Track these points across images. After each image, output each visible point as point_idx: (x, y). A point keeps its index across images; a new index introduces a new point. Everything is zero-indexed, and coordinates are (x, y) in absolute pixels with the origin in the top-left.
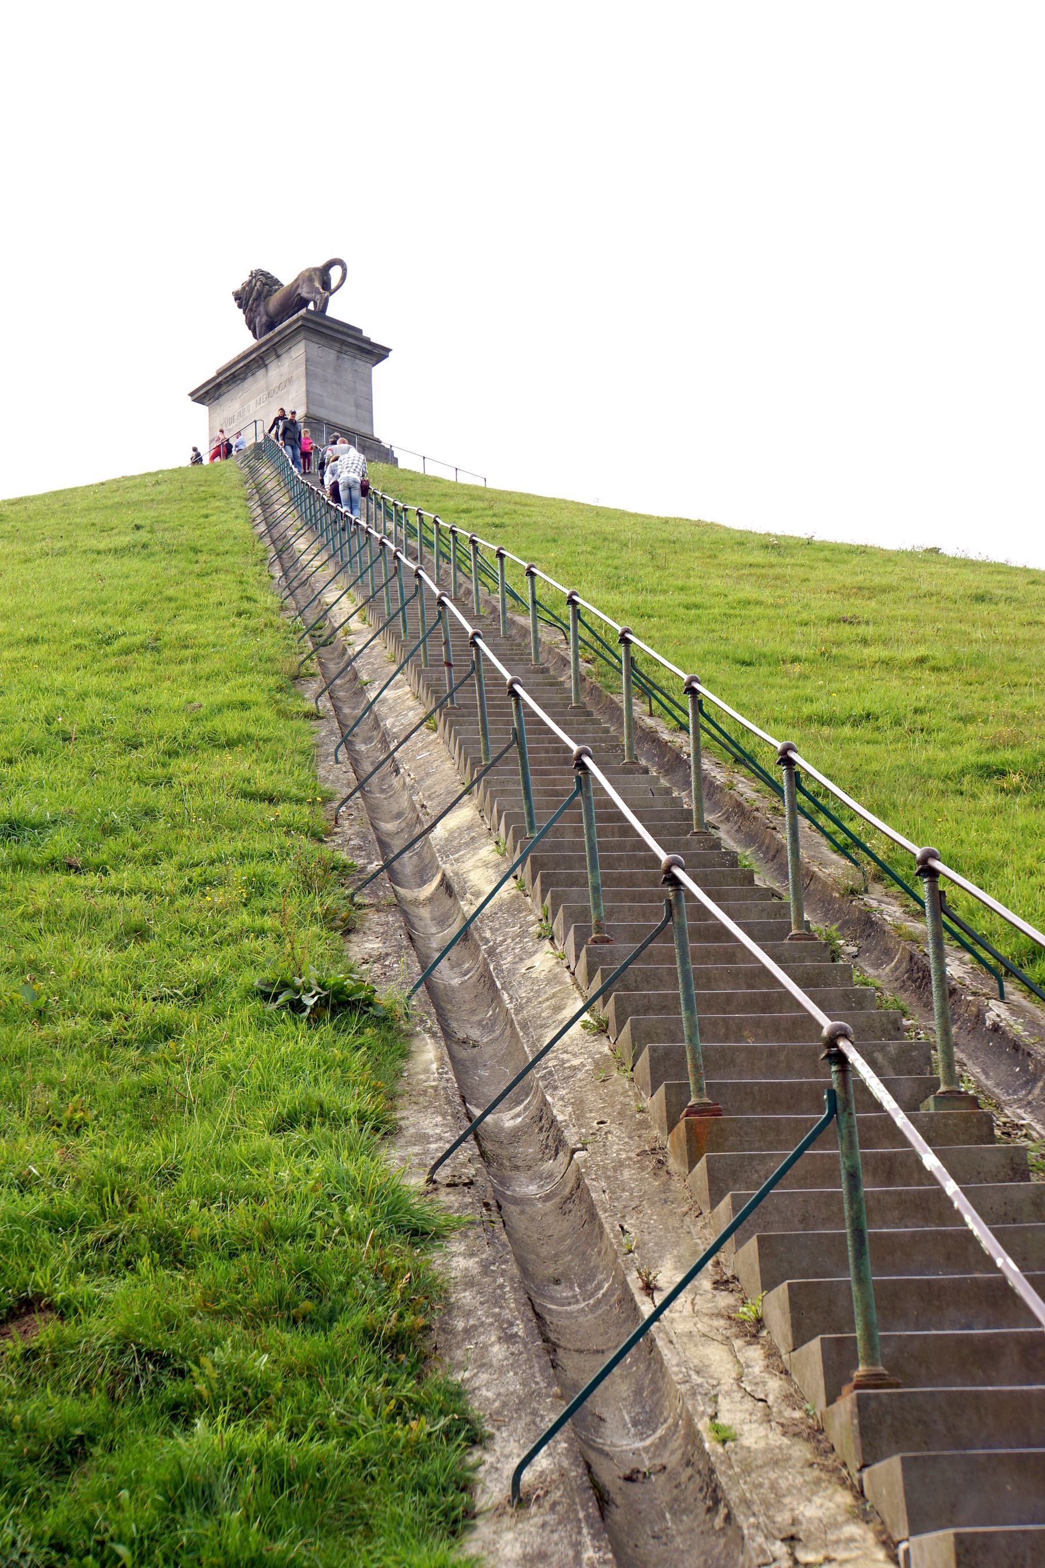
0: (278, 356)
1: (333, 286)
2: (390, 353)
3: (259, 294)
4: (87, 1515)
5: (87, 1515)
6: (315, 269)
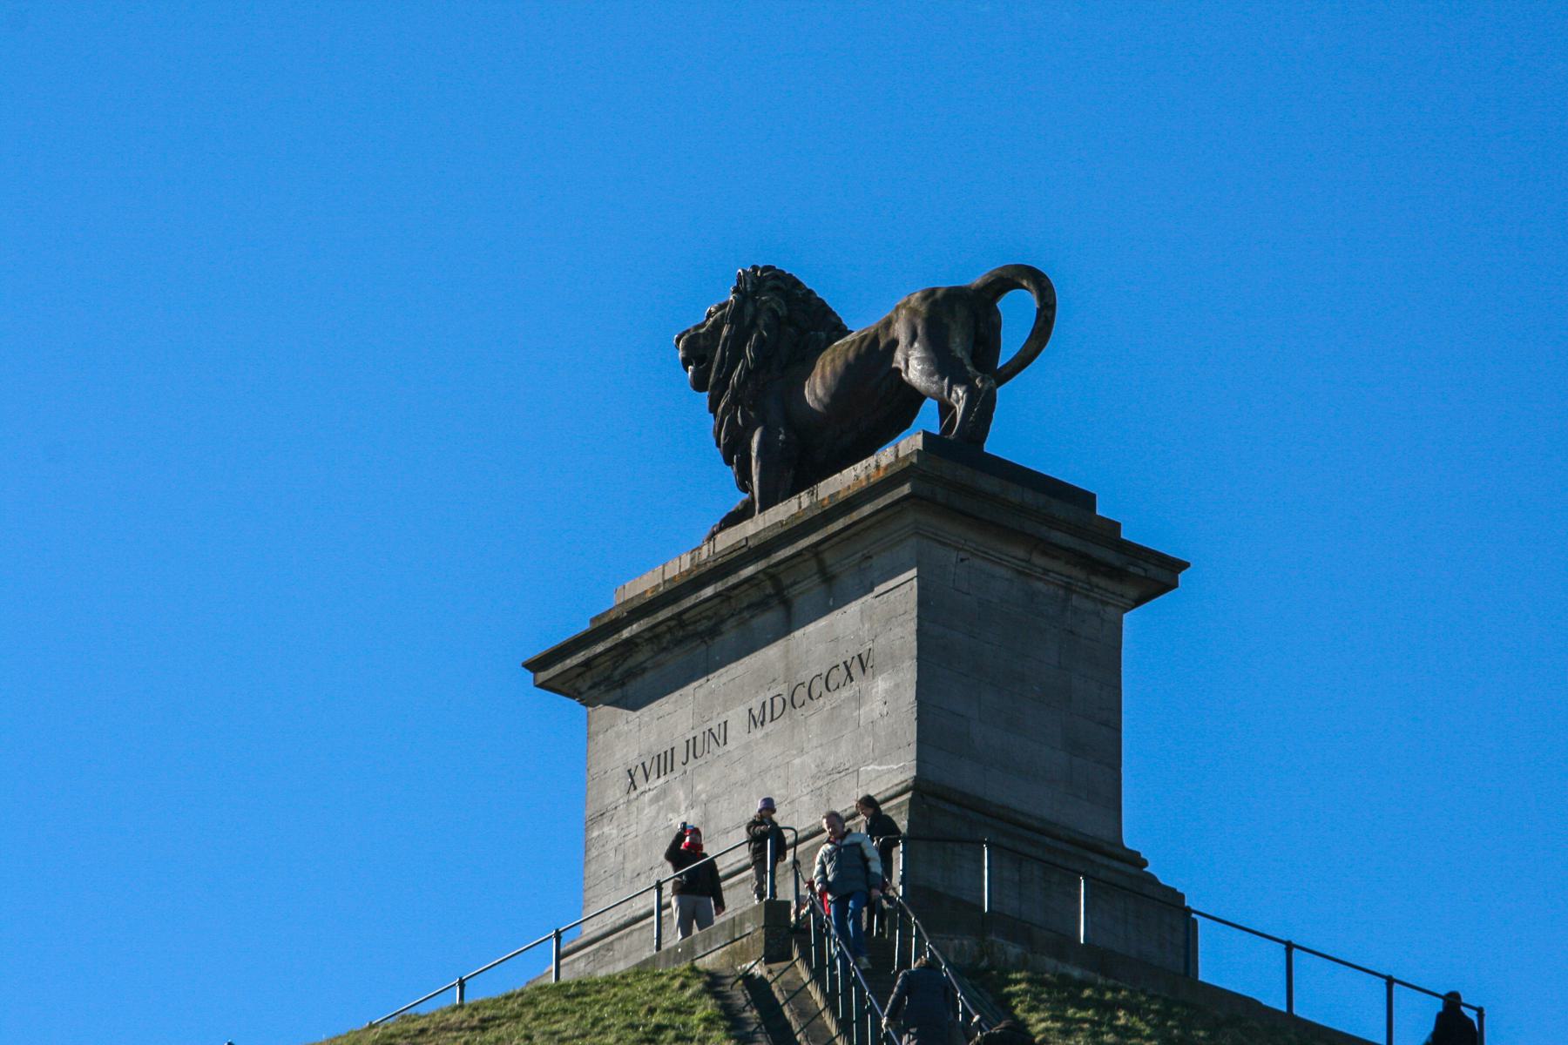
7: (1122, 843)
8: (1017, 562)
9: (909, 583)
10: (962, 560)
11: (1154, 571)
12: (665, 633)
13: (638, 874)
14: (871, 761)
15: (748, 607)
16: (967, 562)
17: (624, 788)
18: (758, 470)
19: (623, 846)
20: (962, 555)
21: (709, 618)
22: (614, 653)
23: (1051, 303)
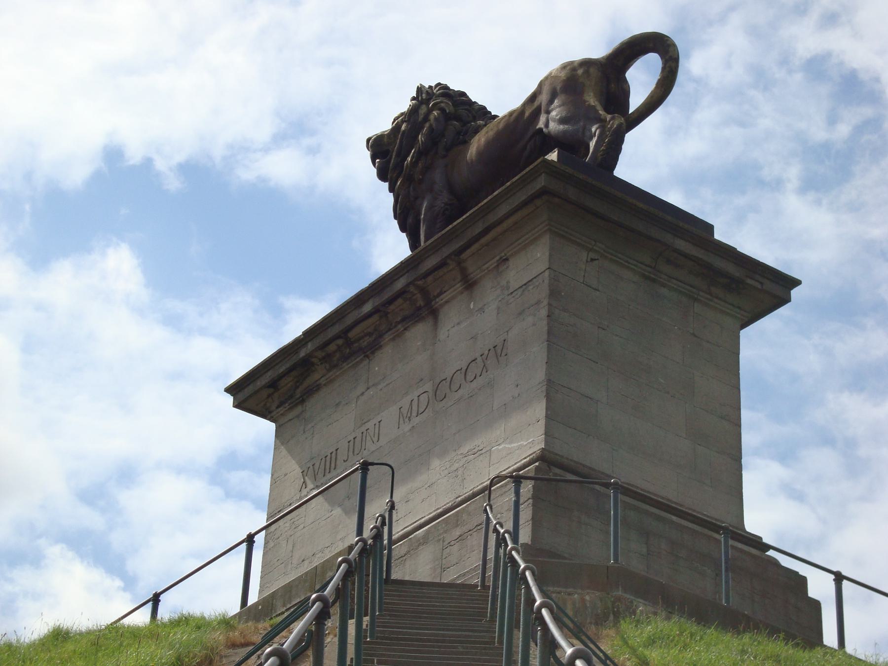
0: (470, 285)
1: (636, 101)
2: (795, 293)
3: (434, 138)
4: (542, 301)
5: (542, 301)
6: (587, 64)
7: (745, 528)
8: (644, 267)
9: (541, 275)
10: (592, 260)
11: (769, 285)
12: (335, 352)
13: (303, 561)
14: (502, 440)
15: (403, 320)
16: (596, 262)
17: (298, 487)
18: (424, 228)
19: (293, 536)
20: (592, 255)
21: (369, 334)
22: (294, 373)
23: (677, 57)
